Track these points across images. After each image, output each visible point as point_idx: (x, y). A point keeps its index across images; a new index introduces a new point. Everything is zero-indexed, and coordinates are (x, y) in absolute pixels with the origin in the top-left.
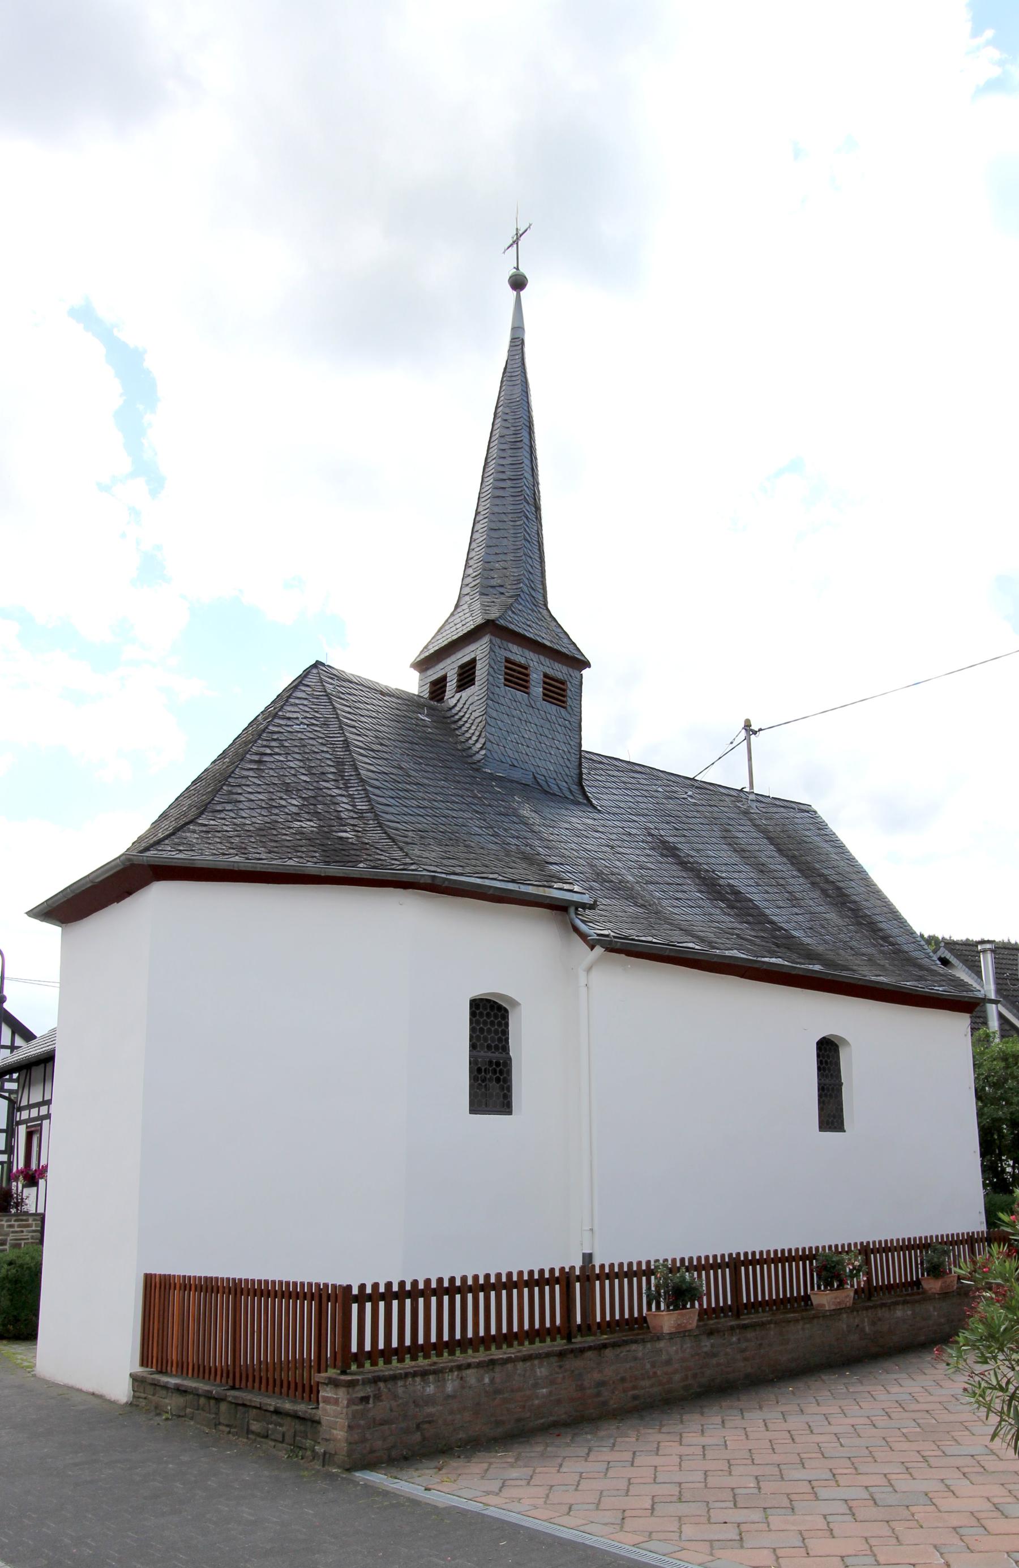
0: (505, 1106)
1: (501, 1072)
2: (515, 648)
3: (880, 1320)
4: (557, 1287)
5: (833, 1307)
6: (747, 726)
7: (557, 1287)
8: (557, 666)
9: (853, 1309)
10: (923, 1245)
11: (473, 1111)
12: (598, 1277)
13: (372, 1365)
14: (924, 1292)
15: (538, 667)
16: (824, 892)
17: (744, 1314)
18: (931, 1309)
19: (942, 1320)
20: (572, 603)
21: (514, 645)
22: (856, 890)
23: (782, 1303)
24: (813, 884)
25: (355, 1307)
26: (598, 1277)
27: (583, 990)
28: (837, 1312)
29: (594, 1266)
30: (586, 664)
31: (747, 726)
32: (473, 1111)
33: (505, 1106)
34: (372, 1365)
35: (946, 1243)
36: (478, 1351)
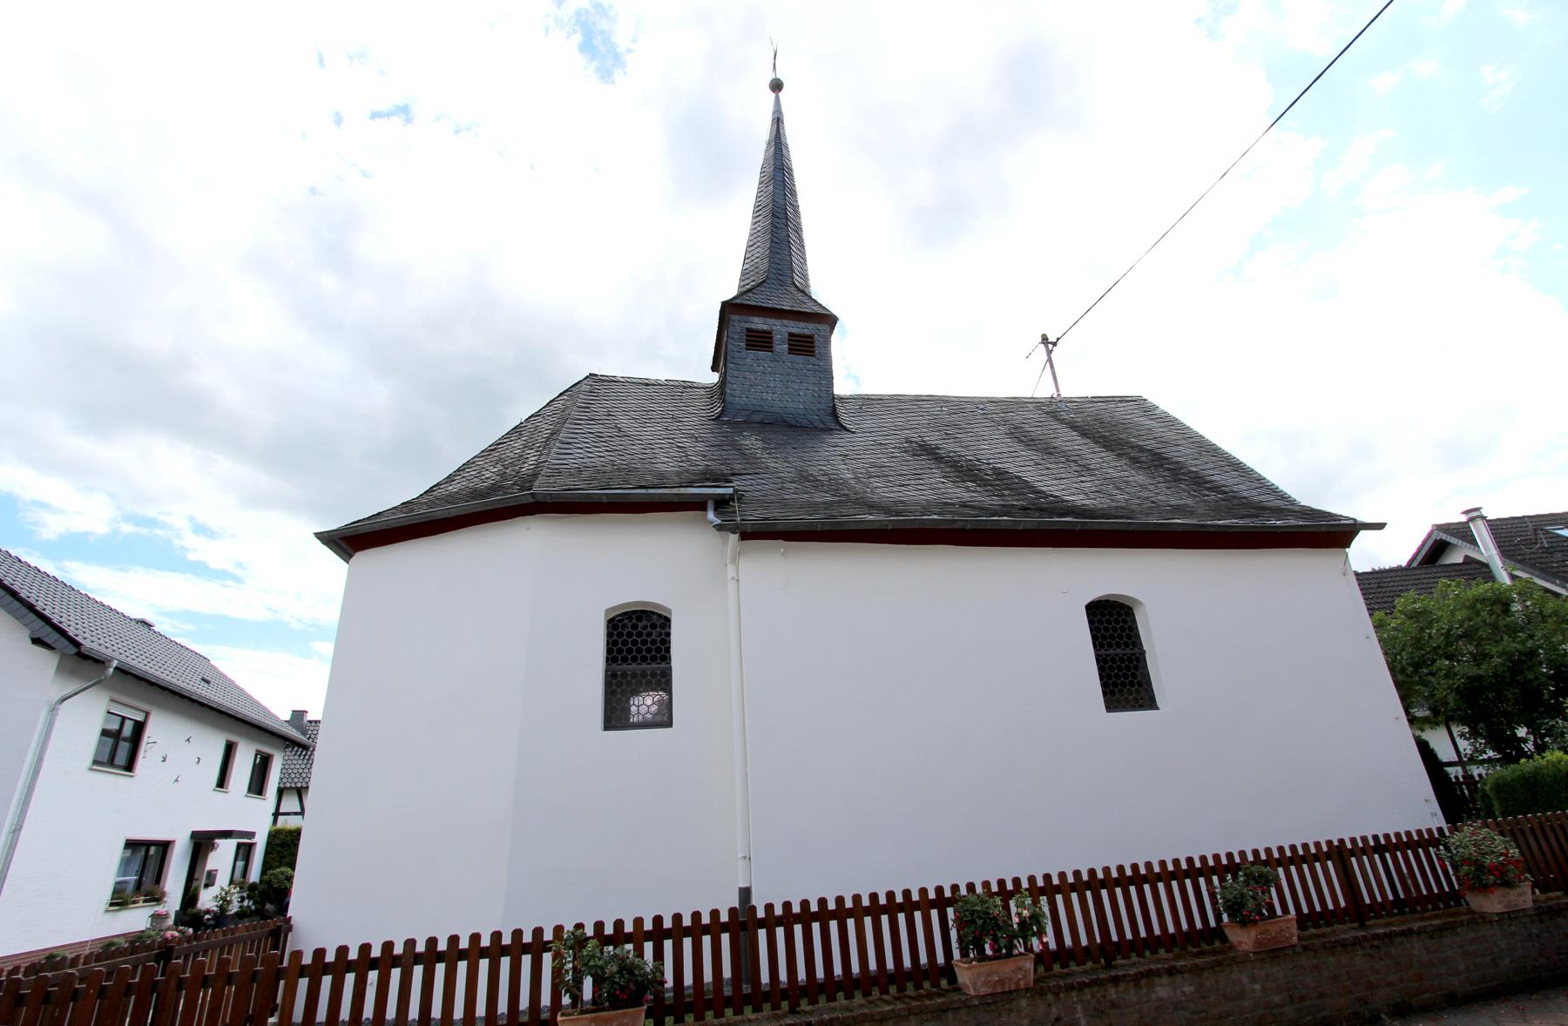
0: (1145, 699)
1: (1136, 668)
2: (756, 319)
3: (1113, 1005)
4: (1330, 863)
5: (984, 990)
6: (1045, 340)
7: (1330, 863)
8: (802, 324)
9: (1037, 990)
10: (1226, 868)
11: (1111, 706)
12: (762, 923)
13: (716, 1017)
14: (1232, 948)
15: (781, 329)
16: (1134, 460)
17: (1370, 918)
18: (1245, 980)
19: (1277, 999)
20: (826, 279)
21: (774, 321)
22: (1182, 454)
23: (1191, 939)
24: (1119, 455)
25: (762, 933)
26: (762, 923)
27: (731, 585)
28: (1002, 998)
29: (754, 908)
30: (829, 320)
31: (1045, 340)
32: (1111, 706)
33: (1145, 699)
34: (716, 1017)
35: (1265, 863)
36: (817, 1002)
